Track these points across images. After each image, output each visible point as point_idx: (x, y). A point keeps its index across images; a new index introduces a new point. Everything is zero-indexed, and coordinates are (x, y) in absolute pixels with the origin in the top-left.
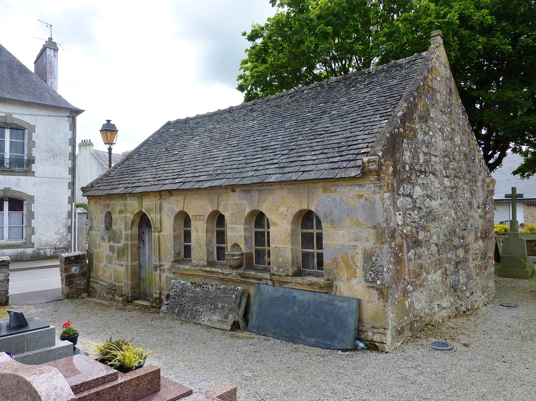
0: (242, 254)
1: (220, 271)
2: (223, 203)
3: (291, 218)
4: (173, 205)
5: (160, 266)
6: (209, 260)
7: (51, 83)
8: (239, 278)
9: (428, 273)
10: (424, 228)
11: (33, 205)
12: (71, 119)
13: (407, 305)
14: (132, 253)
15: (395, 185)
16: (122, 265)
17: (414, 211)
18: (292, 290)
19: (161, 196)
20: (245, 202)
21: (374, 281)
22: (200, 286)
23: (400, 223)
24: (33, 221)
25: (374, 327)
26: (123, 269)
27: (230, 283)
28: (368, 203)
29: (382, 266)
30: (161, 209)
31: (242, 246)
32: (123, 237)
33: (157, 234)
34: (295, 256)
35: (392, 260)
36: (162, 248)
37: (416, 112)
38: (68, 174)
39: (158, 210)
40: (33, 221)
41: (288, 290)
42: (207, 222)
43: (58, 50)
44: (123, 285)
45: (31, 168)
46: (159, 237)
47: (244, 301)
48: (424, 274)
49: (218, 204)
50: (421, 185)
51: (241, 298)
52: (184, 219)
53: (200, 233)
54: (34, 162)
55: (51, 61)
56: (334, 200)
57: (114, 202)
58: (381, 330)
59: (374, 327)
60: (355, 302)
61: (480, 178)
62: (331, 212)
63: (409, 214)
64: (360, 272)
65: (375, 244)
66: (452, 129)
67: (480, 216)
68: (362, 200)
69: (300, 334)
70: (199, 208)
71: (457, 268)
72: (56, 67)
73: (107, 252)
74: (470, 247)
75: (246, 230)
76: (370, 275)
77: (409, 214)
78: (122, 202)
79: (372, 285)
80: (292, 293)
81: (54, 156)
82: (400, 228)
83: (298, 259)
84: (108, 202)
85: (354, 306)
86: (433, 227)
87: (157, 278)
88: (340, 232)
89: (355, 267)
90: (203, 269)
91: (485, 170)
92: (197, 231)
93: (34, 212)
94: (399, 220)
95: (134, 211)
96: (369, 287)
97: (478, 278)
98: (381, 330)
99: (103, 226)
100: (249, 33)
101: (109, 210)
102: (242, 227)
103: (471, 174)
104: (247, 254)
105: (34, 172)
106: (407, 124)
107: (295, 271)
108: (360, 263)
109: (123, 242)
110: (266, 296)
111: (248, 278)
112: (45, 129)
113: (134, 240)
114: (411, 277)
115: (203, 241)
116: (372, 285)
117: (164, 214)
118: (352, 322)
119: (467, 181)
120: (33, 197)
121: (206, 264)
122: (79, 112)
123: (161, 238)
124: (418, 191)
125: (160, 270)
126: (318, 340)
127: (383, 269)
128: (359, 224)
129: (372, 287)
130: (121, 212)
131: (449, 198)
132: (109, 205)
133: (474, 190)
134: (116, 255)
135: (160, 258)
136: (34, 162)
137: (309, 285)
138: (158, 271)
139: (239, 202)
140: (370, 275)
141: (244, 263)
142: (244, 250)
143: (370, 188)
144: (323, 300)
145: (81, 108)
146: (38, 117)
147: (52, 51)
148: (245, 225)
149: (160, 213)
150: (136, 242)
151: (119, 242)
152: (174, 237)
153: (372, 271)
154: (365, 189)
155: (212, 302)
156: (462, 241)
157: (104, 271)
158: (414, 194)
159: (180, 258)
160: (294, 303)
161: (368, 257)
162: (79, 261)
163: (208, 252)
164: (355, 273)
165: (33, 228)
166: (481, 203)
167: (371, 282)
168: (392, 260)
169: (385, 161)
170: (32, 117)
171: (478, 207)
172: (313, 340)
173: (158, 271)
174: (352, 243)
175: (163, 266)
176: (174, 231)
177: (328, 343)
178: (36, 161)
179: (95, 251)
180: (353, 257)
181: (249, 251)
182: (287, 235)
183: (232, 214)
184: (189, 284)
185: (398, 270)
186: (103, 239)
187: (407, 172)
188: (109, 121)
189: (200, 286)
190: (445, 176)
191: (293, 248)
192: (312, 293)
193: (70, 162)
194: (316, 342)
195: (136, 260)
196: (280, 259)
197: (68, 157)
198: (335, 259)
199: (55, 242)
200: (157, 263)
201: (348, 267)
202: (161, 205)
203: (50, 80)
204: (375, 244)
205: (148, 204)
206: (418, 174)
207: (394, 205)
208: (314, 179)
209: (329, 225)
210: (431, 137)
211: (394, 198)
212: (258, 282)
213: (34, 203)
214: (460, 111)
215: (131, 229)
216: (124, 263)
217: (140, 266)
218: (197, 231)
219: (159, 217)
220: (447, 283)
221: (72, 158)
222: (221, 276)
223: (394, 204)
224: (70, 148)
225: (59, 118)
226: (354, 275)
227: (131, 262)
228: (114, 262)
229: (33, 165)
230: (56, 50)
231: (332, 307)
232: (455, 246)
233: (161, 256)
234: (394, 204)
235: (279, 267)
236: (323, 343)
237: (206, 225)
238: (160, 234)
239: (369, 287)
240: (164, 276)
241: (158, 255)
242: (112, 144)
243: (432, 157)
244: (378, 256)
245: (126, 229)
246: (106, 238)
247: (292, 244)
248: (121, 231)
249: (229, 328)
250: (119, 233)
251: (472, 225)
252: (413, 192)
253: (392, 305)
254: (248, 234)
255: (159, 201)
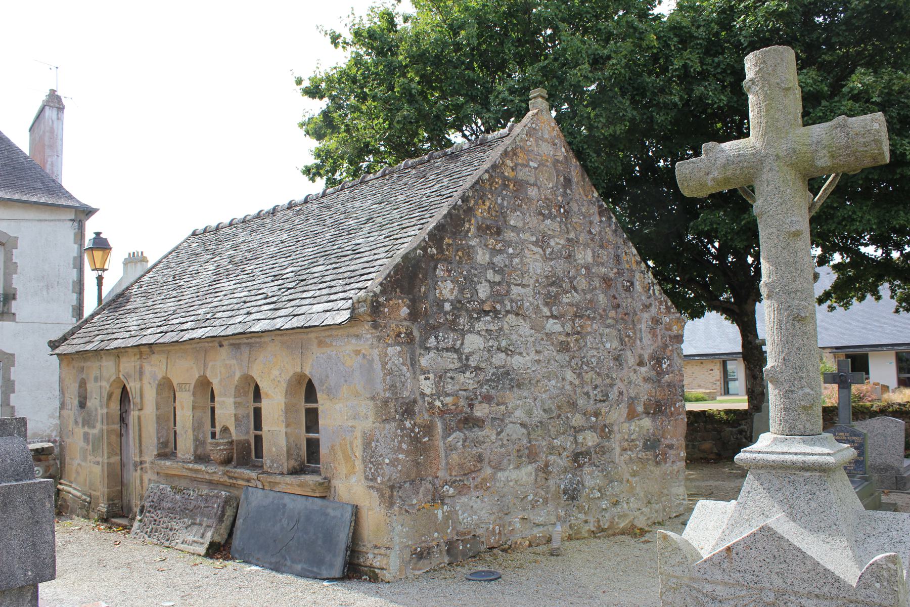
0: (231, 443)
1: (204, 468)
2: (210, 364)
3: (285, 385)
4: (155, 368)
5: (141, 463)
6: (198, 452)
7: (52, 164)
8: (226, 479)
9: (498, 468)
10: (488, 399)
11: (12, 369)
12: (76, 224)
13: (440, 516)
14: (109, 444)
15: (416, 333)
16: (98, 463)
17: (464, 373)
18: (283, 495)
19: (141, 353)
20: (235, 362)
21: (374, 479)
22: (180, 491)
23: (428, 391)
24: (12, 395)
25: (376, 547)
26: (97, 470)
27: (220, 487)
28: (366, 361)
29: (381, 456)
30: (141, 373)
31: (232, 429)
32: (99, 418)
33: (136, 413)
34: (293, 445)
35: (404, 446)
36: (143, 435)
37: (470, 221)
38: (70, 317)
39: (138, 376)
40: (12, 395)
41: (279, 494)
42: (194, 394)
43: (64, 108)
44: (98, 494)
45: (9, 308)
46: (139, 418)
47: (229, 512)
48: (488, 471)
49: (205, 366)
50: (483, 333)
51: (224, 507)
52: (167, 388)
53: (146, 412)
54: (14, 298)
55: (52, 128)
56: (330, 357)
57: (88, 364)
58: (383, 551)
59: (376, 547)
60: (349, 509)
61: (646, 315)
62: (327, 376)
63: (452, 378)
64: (359, 465)
65: (374, 423)
66: (569, 240)
67: (644, 378)
68: (360, 358)
69: (286, 559)
70: (184, 372)
71: (575, 461)
72: (59, 138)
73: (81, 443)
74: (616, 428)
75: (237, 405)
76: (370, 469)
77: (452, 378)
78: (97, 364)
79: (372, 484)
80: (283, 498)
81: (47, 287)
82: (427, 399)
83: (300, 449)
84: (82, 364)
85: (348, 515)
86: (512, 398)
87: (138, 482)
88: (337, 407)
89: (353, 458)
90: (186, 466)
91: (661, 303)
92: (182, 409)
93: (14, 381)
94: (427, 387)
95: (110, 377)
96: (370, 487)
97: (634, 480)
98: (383, 551)
99: (76, 402)
100: (306, 84)
101: (84, 376)
102: (232, 400)
103: (620, 310)
104: (239, 442)
105: (14, 314)
106: (446, 240)
107: (294, 468)
108: (359, 452)
109: (99, 426)
110: (253, 504)
111: (236, 478)
112: (39, 242)
113: (113, 423)
114: (453, 474)
115: (189, 424)
116: (372, 484)
117: (145, 381)
118: (343, 538)
119: (609, 321)
120: (13, 355)
121: (192, 458)
122: (89, 212)
123: (142, 419)
124: (473, 342)
125: (142, 469)
126: (305, 566)
127: (383, 461)
128: (357, 395)
129: (372, 487)
130: (96, 379)
131: (558, 351)
132: (83, 368)
133: (629, 336)
134: (90, 447)
135: (141, 452)
136: (14, 298)
137: (299, 486)
138: (139, 471)
139: (227, 362)
140: (370, 469)
141: (235, 455)
142: (235, 435)
143: (367, 340)
144: (316, 508)
145: (94, 206)
146: (22, 223)
147: (55, 112)
148: (235, 398)
149: (141, 379)
150: (117, 427)
151: (94, 427)
152: (158, 418)
153: (372, 463)
154: (362, 342)
155: (188, 513)
156: (593, 419)
157: (78, 473)
158: (465, 346)
159: (167, 450)
160: (284, 513)
161: (368, 442)
162: (43, 457)
163: (196, 439)
164: (354, 467)
165: (13, 407)
166: (646, 357)
167: (371, 480)
168: (404, 446)
169: (388, 300)
170: (13, 223)
171: (641, 363)
172: (299, 567)
173: (139, 471)
174: (351, 423)
175: (145, 462)
176: (157, 409)
177: (315, 570)
178: (18, 297)
179: (68, 441)
180: (351, 443)
181: (243, 437)
182: (281, 413)
183: (221, 381)
184: (169, 489)
185: (418, 463)
186: (76, 422)
187: (446, 313)
188: (98, 234)
189: (180, 491)
190: (548, 317)
191: (289, 430)
192: (304, 498)
193: (75, 296)
194: (302, 569)
195: (116, 454)
196: (274, 449)
197: (71, 288)
198: (333, 446)
199: (48, 432)
200: (138, 459)
201: (347, 458)
202: (141, 368)
203: (49, 160)
204: (374, 423)
205: (128, 365)
206: (475, 316)
207: (412, 365)
208: (298, 328)
209: (325, 396)
210: (511, 257)
211: (413, 354)
212: (247, 484)
213: (13, 365)
214: (594, 209)
215: (108, 406)
216: (100, 460)
217: (122, 465)
218: (182, 409)
219: (138, 386)
220: (548, 487)
221: (77, 290)
222: (207, 477)
223: (414, 363)
224: (74, 274)
225: (57, 223)
226: (352, 471)
227: (109, 458)
228: (89, 458)
229: (13, 302)
230: (61, 108)
231: (323, 519)
232: (575, 428)
233: (143, 447)
234: (414, 363)
235: (272, 461)
236: (309, 571)
237: (192, 398)
238: (142, 412)
239: (370, 487)
240: (146, 478)
241: (137, 445)
242: (104, 270)
243: (513, 287)
244: (377, 441)
245: (101, 407)
246: (80, 420)
247: (287, 426)
248: (96, 409)
249: (202, 550)
250: (94, 413)
251: (621, 393)
252: (462, 344)
253: (400, 514)
254: (241, 412)
255: (139, 362)
